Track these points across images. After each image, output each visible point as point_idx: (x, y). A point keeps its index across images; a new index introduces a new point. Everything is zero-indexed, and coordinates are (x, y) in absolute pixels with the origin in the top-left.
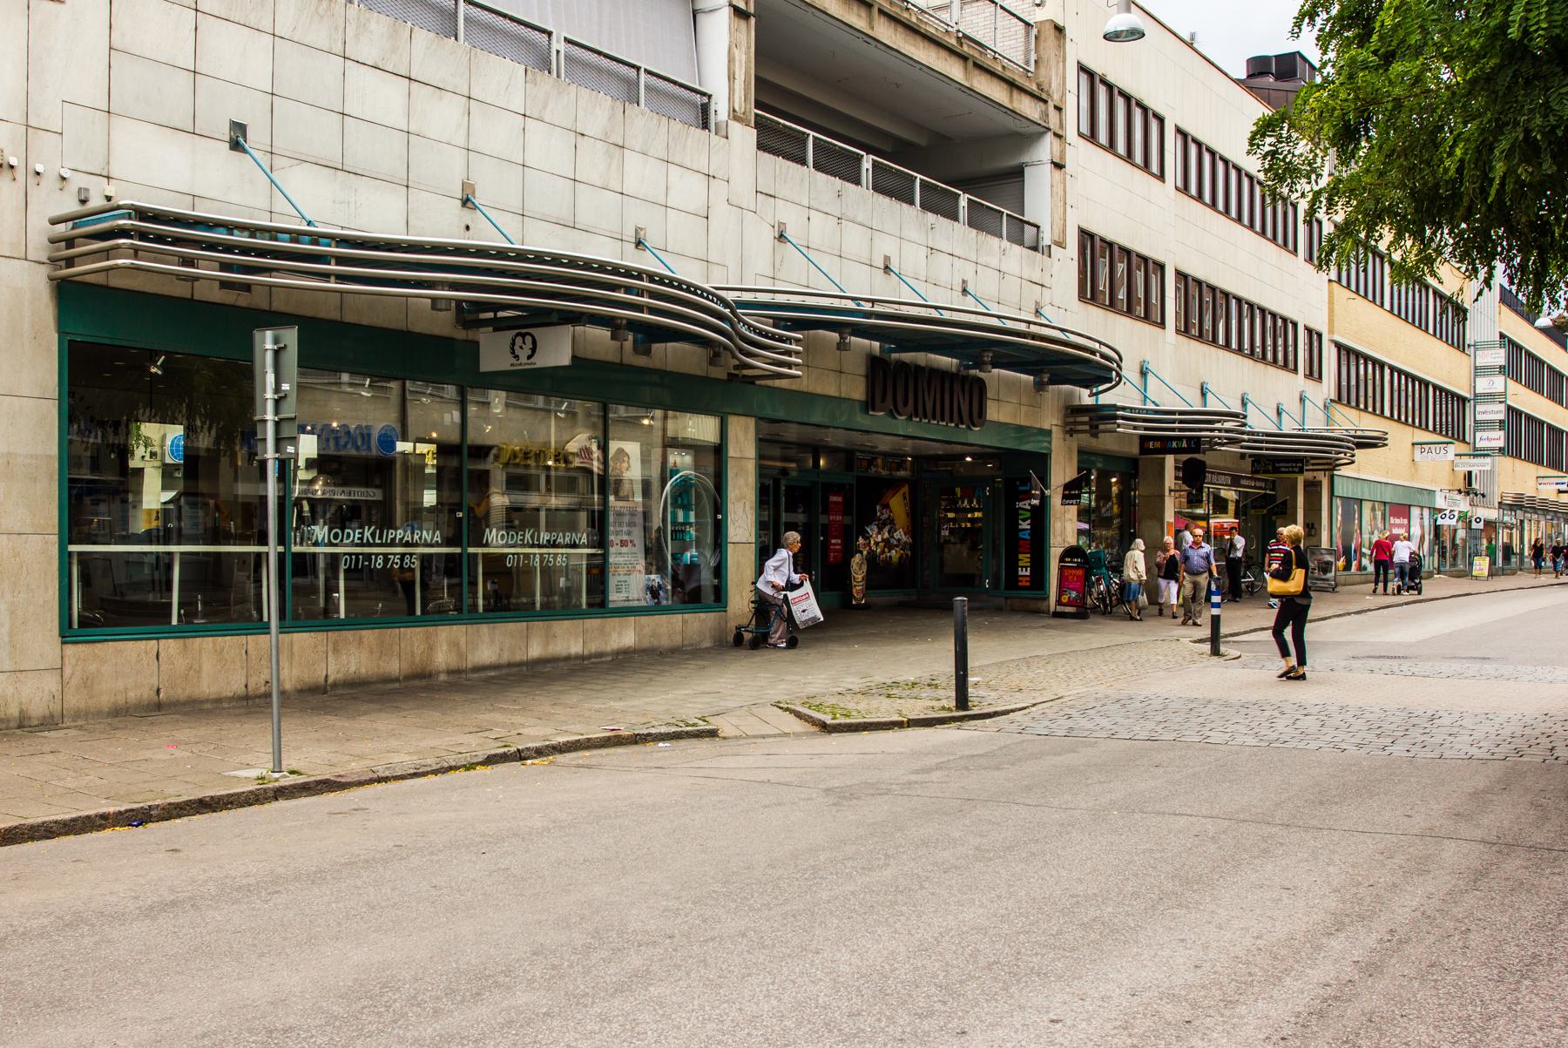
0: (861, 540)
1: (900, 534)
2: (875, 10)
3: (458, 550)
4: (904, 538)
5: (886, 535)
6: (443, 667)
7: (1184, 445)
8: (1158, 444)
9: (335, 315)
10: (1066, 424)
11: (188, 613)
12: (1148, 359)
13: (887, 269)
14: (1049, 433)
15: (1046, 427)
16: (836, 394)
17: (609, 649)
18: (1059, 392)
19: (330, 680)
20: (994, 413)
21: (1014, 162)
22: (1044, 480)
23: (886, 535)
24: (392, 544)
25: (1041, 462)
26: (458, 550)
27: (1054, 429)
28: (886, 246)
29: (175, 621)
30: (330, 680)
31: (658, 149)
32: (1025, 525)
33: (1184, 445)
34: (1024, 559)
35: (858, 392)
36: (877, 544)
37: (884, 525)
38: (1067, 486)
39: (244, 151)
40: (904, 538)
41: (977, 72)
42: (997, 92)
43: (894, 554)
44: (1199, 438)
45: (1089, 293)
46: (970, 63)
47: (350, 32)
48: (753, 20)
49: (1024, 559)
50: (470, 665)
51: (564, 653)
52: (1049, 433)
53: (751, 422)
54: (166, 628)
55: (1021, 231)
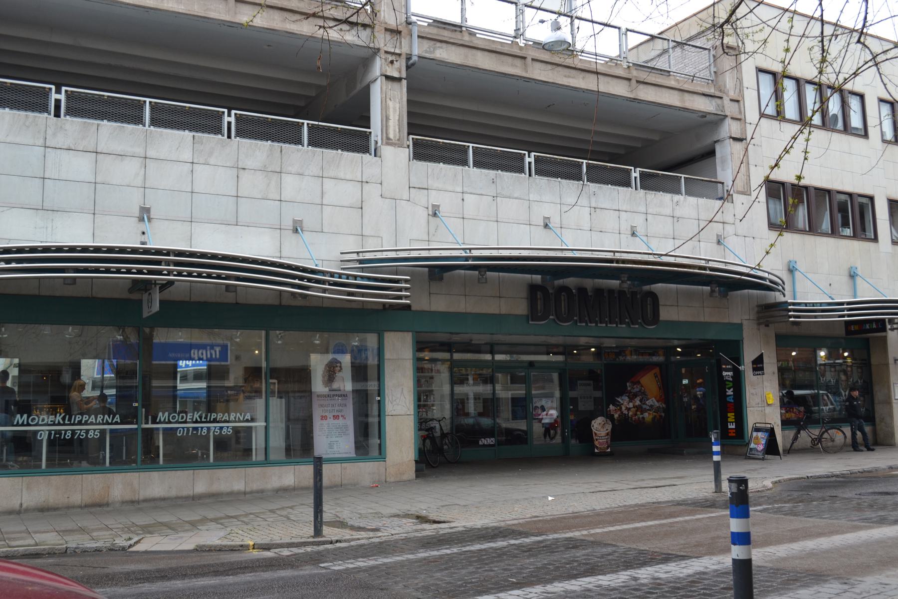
0: (611, 407)
1: (652, 402)
2: (529, 60)
3: (135, 426)
4: (657, 404)
5: (638, 403)
6: (119, 498)
7: (874, 326)
8: (857, 327)
9: (36, 292)
10: (758, 319)
11: (143, 462)
12: (858, 265)
13: (546, 226)
14: (740, 326)
15: (736, 320)
16: (497, 312)
17: (269, 486)
18: (750, 297)
19: (24, 506)
20: (666, 314)
21: (708, 141)
22: (738, 360)
23: (638, 403)
24: (215, 421)
25: (734, 349)
26: (135, 426)
27: (745, 323)
28: (550, 211)
29: (44, 466)
30: (24, 506)
31: (314, 170)
32: (730, 392)
33: (874, 326)
34: (731, 416)
35: (521, 308)
36: (628, 409)
37: (635, 395)
38: (754, 362)
39: (637, 236)
40: (657, 404)
41: (641, 86)
42: (673, 99)
43: (648, 416)
44: (884, 320)
45: (783, 225)
46: (633, 82)
47: (49, 132)
48: (404, 82)
49: (731, 416)
50: (141, 498)
51: (229, 490)
52: (740, 326)
53: (410, 334)
54: (156, 466)
55: (711, 188)
